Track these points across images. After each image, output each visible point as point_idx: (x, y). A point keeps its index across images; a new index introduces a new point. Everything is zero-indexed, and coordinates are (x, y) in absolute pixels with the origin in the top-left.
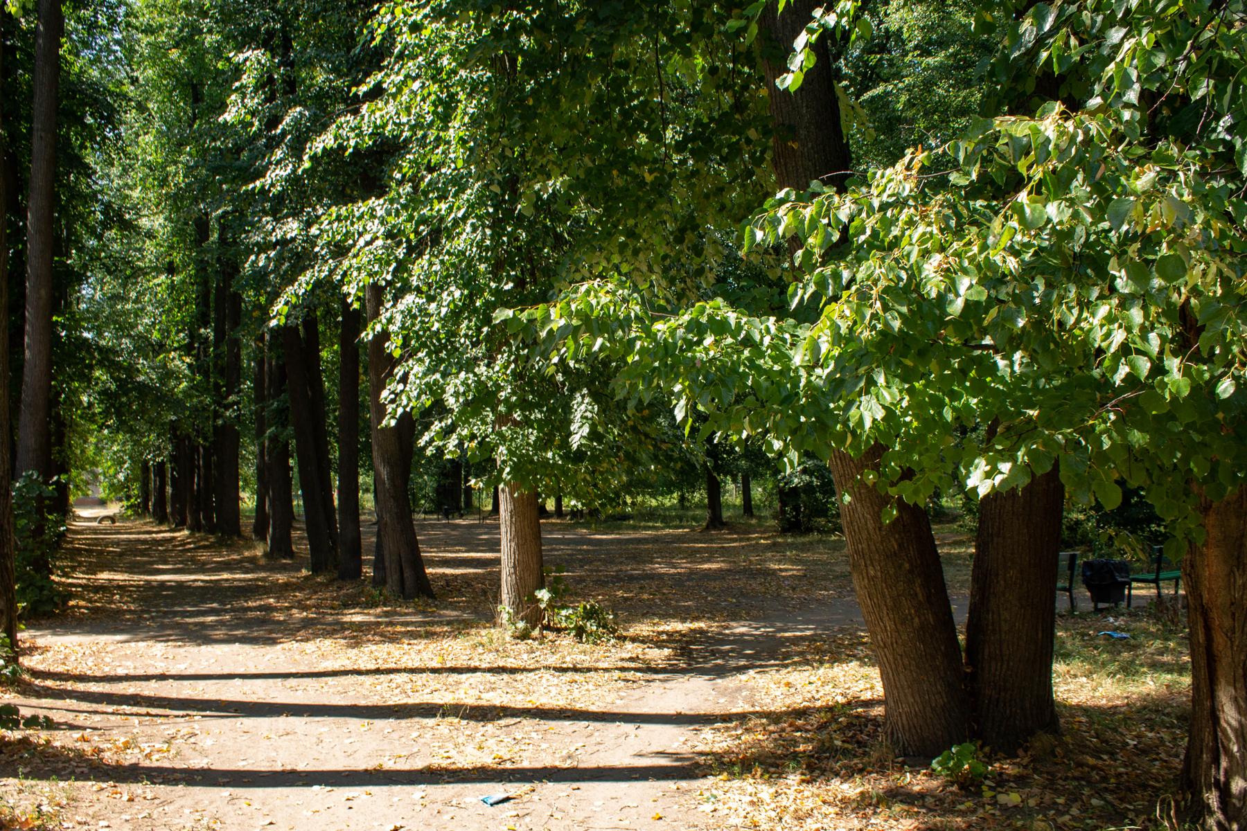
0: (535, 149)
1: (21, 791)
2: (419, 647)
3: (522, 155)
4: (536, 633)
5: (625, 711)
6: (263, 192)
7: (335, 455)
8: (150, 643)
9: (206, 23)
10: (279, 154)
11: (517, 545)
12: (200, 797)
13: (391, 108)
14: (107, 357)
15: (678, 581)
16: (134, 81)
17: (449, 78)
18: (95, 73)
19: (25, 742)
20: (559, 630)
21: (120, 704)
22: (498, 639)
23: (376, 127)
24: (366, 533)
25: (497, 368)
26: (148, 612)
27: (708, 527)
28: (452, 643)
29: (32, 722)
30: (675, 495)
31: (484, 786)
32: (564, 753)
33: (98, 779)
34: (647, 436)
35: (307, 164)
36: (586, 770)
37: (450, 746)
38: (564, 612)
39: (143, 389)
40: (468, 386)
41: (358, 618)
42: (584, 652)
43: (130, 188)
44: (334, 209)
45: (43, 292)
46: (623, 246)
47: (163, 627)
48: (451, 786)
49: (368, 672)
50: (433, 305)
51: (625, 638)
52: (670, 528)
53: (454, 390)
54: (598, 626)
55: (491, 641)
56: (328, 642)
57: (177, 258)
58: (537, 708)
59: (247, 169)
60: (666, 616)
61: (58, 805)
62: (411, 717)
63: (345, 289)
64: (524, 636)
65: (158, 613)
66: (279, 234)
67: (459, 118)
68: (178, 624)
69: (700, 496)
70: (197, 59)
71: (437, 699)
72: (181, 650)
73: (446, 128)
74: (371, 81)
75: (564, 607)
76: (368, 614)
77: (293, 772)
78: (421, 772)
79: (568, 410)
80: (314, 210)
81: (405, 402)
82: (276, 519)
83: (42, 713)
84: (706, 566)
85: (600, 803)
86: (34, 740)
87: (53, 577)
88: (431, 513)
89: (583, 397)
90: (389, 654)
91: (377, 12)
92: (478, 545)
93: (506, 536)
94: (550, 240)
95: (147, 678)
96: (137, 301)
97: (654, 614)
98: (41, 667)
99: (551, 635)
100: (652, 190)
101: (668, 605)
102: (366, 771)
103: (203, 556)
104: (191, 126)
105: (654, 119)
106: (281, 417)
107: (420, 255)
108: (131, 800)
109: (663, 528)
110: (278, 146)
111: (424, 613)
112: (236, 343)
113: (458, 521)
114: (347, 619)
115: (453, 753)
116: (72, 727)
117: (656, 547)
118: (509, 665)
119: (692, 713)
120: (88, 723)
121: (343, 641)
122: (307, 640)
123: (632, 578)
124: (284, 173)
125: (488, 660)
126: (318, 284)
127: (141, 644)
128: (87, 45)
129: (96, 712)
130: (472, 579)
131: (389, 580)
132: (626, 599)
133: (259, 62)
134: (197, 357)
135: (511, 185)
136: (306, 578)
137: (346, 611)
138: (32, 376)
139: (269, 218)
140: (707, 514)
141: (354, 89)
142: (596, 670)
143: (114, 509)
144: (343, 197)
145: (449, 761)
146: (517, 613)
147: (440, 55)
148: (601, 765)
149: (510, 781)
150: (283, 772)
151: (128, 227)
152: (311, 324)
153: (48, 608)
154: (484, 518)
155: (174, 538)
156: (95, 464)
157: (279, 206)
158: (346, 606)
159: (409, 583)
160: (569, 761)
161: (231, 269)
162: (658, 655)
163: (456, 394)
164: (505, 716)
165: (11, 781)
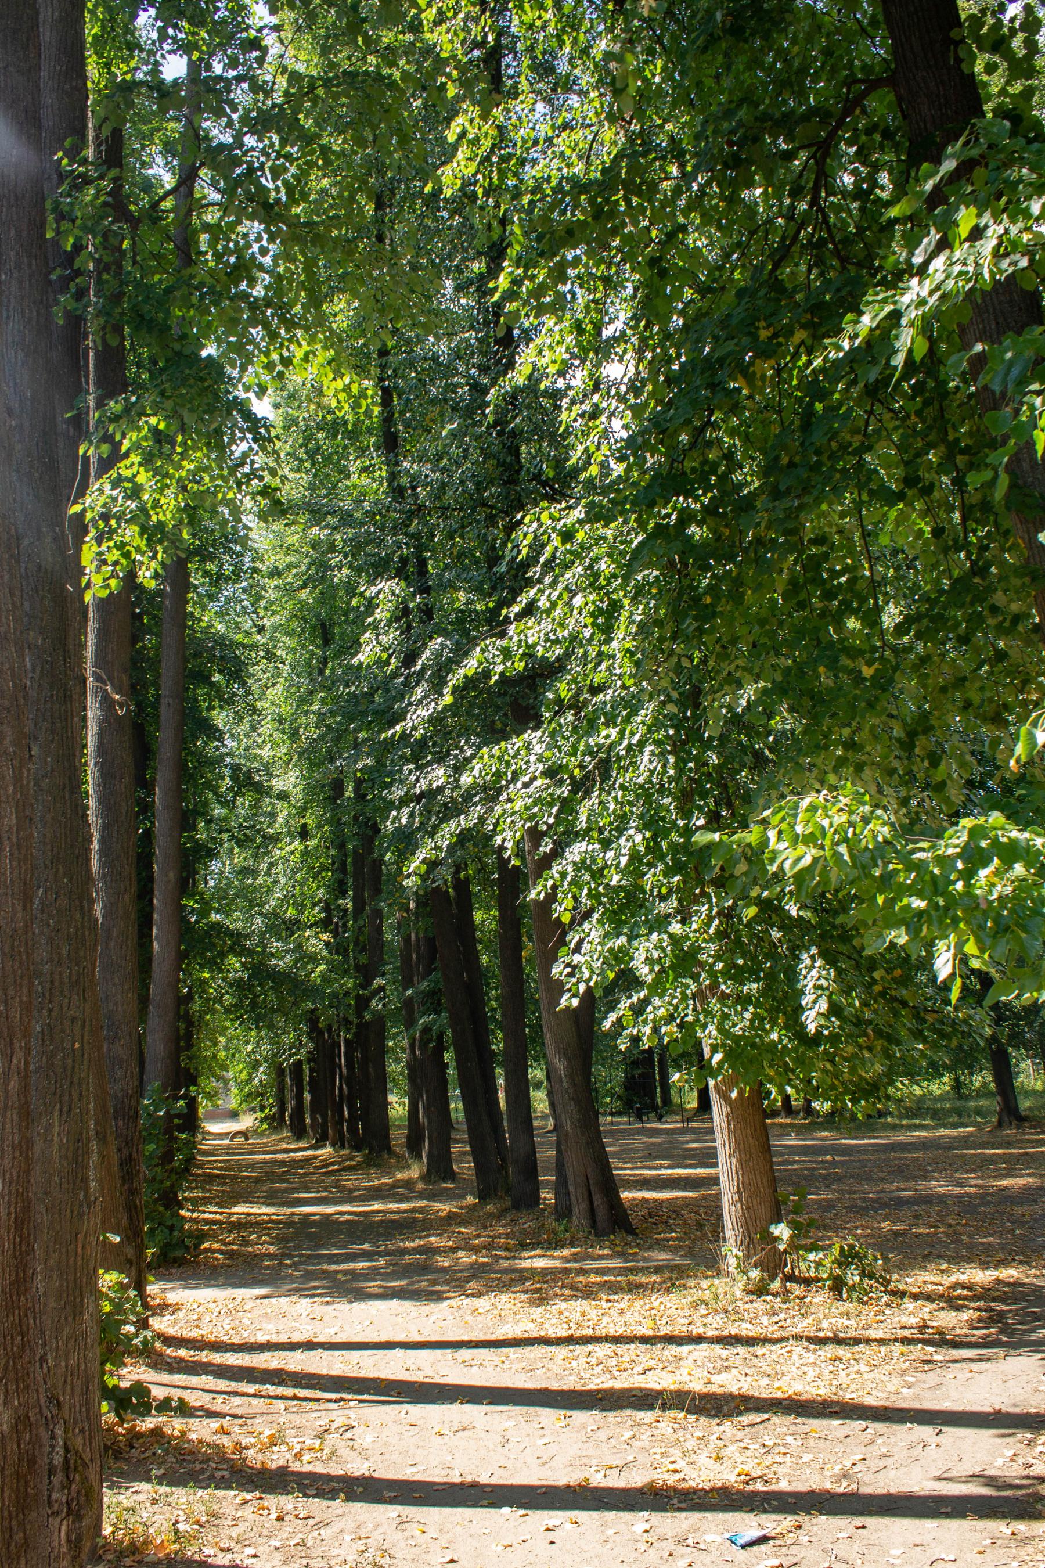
0: (718, 655)
1: (155, 1502)
2: (622, 1305)
3: (704, 661)
4: (776, 1285)
5: (917, 1405)
6: (404, 736)
7: (498, 1045)
8: (293, 1299)
9: (335, 559)
10: (419, 692)
11: (740, 1161)
12: (361, 1518)
13: (546, 625)
14: (237, 942)
15: (967, 1206)
16: (261, 630)
17: (609, 584)
18: (220, 627)
19: (157, 1433)
20: (807, 1282)
21: (263, 1382)
22: (723, 1294)
23: (528, 646)
24: (543, 1144)
25: (695, 926)
26: (290, 1256)
27: (1000, 1124)
28: (664, 1299)
29: (165, 1406)
30: (946, 1079)
31: (729, 1516)
32: (837, 1469)
33: (242, 1487)
34: (904, 1004)
35: (448, 699)
36: (871, 1497)
37: (676, 1453)
38: (812, 1256)
39: (279, 978)
40: (663, 950)
41: (540, 1263)
42: (847, 1314)
43: (260, 747)
44: (485, 750)
45: (171, 874)
46: (842, 762)
47: (309, 1276)
48: (683, 1515)
49: (559, 1341)
50: (610, 854)
51: (903, 1294)
52: (945, 1126)
53: (645, 953)
54: (863, 1275)
55: (716, 1297)
56: (505, 1297)
57: (310, 821)
58: (789, 1398)
59: (384, 713)
60: (957, 1259)
61: (197, 1522)
62: (621, 1408)
63: (498, 840)
64: (760, 1290)
65: (301, 1258)
66: (423, 784)
67: (623, 627)
68: (325, 1272)
69: (982, 1079)
70: (328, 597)
71: (655, 1382)
72: (330, 1308)
73: (608, 641)
74: (523, 600)
75: (813, 1248)
76: (554, 1258)
77: (474, 1485)
78: (640, 1491)
79: (792, 975)
80: (462, 751)
81: (587, 975)
82: (430, 1133)
83: (176, 1394)
84: (1005, 1182)
85: (897, 1552)
86: (167, 1430)
87: (183, 1212)
88: (620, 1114)
89: (813, 958)
90: (583, 1315)
91: (520, 522)
92: (685, 1157)
93: (722, 1142)
94: (748, 759)
95: (292, 1346)
96: (268, 873)
97: (939, 1257)
98: (171, 1331)
99: (798, 1290)
100: (872, 685)
101: (958, 1241)
102: (568, 1487)
103: (350, 1180)
104: (321, 672)
105: (862, 598)
106: (432, 1001)
107: (587, 794)
108: (280, 1519)
109: (935, 1128)
110: (417, 684)
111: (623, 1255)
112: (378, 914)
113: (654, 1125)
114: (526, 1264)
115: (681, 1464)
116: (211, 1414)
117: (929, 1155)
118: (744, 1333)
119: (1017, 1410)
120: (226, 1409)
121: (524, 1297)
122: (479, 1295)
123: (900, 1203)
124: (425, 714)
125: (715, 1325)
126: (464, 837)
127: (283, 1300)
128: (212, 597)
129: (235, 1394)
130: (681, 1207)
131: (575, 1210)
132: (896, 1234)
133: (393, 594)
134: (335, 933)
135: (693, 698)
136: (473, 1208)
137: (524, 1254)
138: (160, 969)
139: (411, 766)
140: (993, 1104)
141: (504, 612)
142: (868, 1341)
143: (247, 1122)
144: (495, 734)
145: (677, 1476)
146: (748, 1257)
147: (597, 559)
148: (893, 1491)
149: (765, 1511)
150: (462, 1484)
151: (261, 790)
152: (462, 886)
153: (179, 1253)
154: (688, 1120)
155: (316, 1157)
156: (225, 1068)
157: (420, 752)
158: (524, 1246)
159: (601, 1214)
160: (845, 1483)
161: (371, 830)
162: (948, 1319)
163: (649, 961)
164: (748, 1410)
165: (145, 1486)
